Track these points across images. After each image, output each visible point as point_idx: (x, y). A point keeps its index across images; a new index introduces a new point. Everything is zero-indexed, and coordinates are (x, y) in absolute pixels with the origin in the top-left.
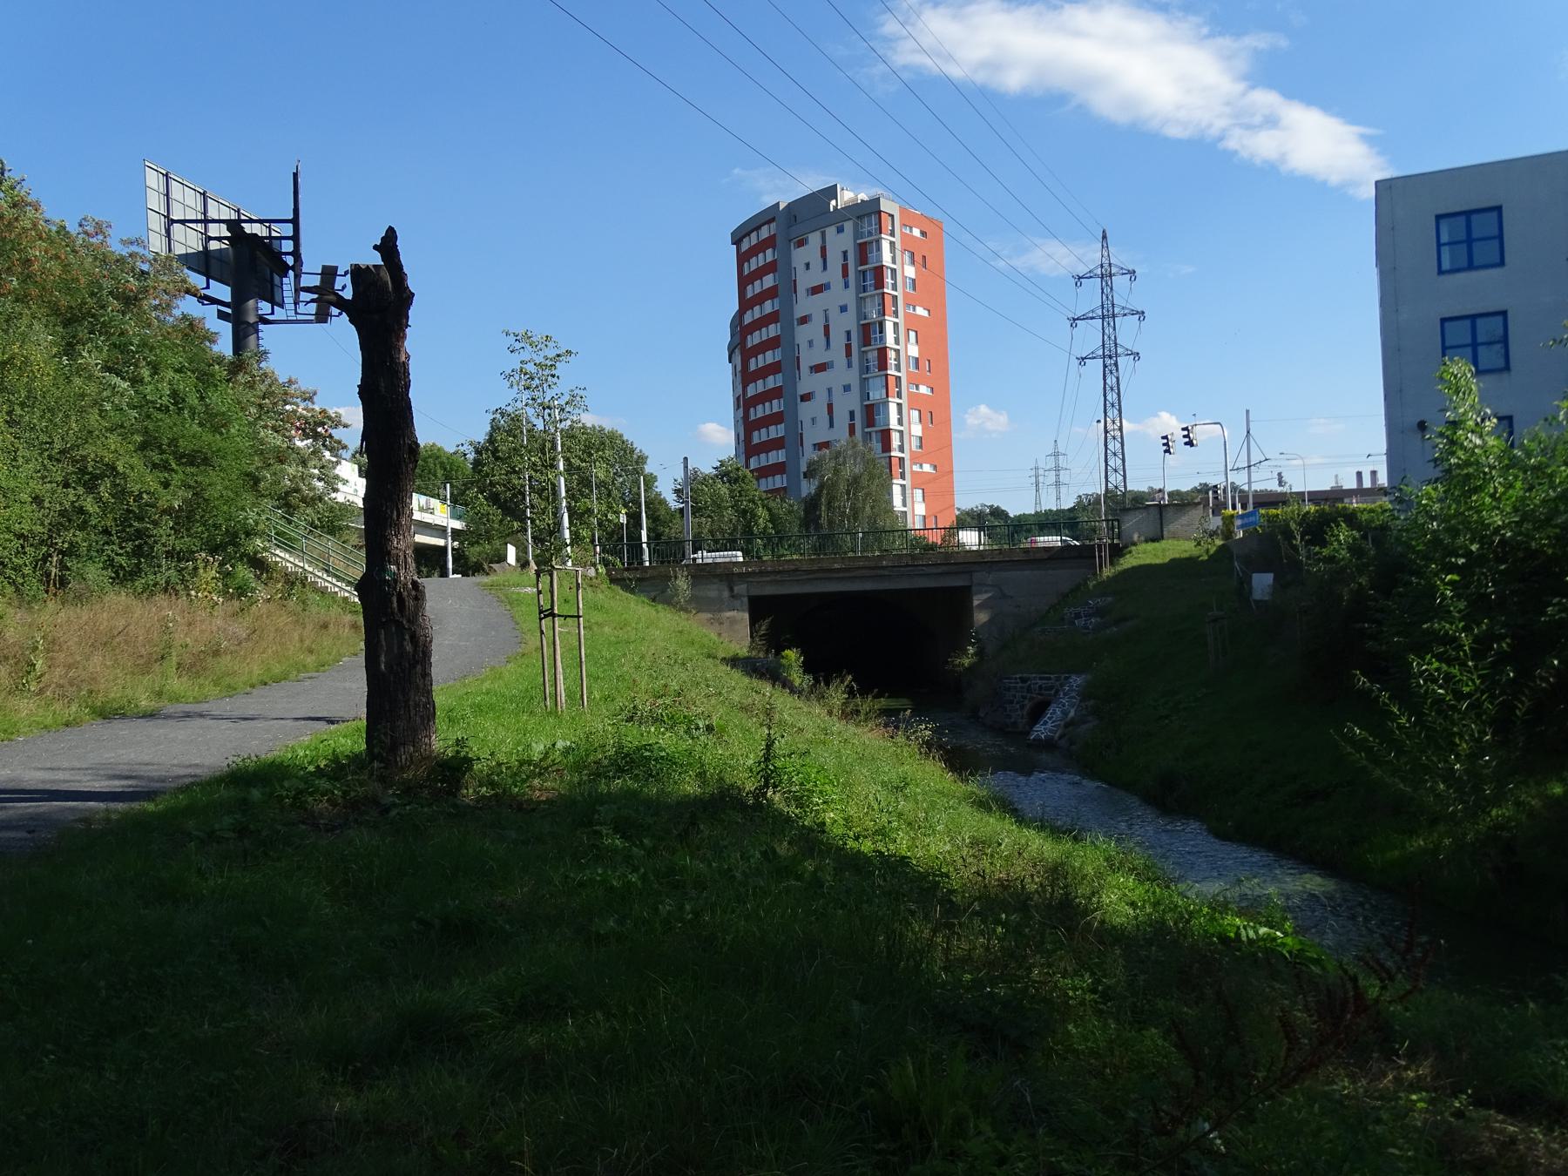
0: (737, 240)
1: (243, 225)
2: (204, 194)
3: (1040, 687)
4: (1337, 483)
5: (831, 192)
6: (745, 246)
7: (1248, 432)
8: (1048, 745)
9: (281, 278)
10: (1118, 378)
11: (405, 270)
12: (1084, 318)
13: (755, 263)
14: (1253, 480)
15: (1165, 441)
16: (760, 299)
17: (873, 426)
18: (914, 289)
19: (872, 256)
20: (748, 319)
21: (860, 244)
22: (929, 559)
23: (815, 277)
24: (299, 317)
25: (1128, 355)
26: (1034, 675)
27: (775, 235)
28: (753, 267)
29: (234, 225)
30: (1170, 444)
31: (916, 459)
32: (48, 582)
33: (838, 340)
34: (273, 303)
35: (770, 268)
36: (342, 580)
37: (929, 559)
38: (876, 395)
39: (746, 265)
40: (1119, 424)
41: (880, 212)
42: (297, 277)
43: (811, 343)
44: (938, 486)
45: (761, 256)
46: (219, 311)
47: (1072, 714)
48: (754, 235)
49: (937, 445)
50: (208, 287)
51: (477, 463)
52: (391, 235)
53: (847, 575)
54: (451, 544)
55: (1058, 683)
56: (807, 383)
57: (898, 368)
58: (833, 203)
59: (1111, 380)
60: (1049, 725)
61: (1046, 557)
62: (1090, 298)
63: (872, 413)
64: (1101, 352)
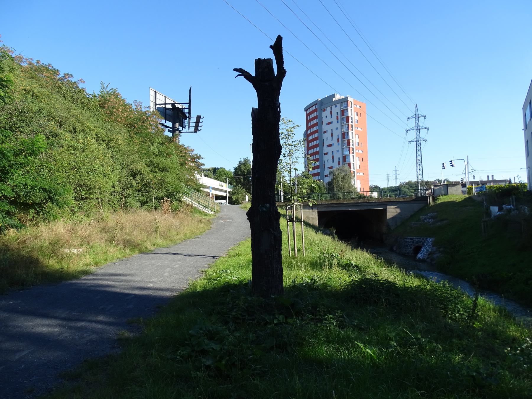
0: (306, 111)
1: (175, 105)
2: (165, 97)
3: (417, 242)
4: (481, 179)
5: (334, 96)
6: (308, 112)
7: (468, 162)
8: (423, 261)
9: (185, 120)
10: (421, 148)
11: (284, 60)
12: (410, 130)
13: (311, 116)
14: (469, 177)
15: (443, 165)
16: (312, 126)
17: (345, 162)
18: (358, 123)
19: (345, 113)
20: (309, 132)
21: (342, 110)
22: (373, 200)
23: (329, 120)
24: (190, 131)
25: (423, 140)
26: (415, 238)
27: (318, 144)
28: (311, 118)
29: (173, 105)
30: (445, 166)
31: (358, 171)
32: (121, 206)
33: (335, 138)
34: (183, 127)
35: (316, 118)
36: (203, 206)
37: (373, 200)
38: (346, 153)
39: (309, 117)
40: (421, 161)
41: (348, 101)
42: (189, 119)
43: (327, 138)
44: (364, 179)
45: (313, 114)
46: (168, 129)
47: (430, 250)
48: (311, 108)
49: (364, 168)
50: (166, 123)
51: (235, 173)
52: (279, 39)
53: (348, 205)
54: (228, 195)
55: (423, 240)
56: (325, 128)
57: (353, 145)
58: (334, 99)
59: (419, 148)
60: (423, 254)
61: (410, 200)
62: (412, 123)
63: (345, 158)
64: (415, 140)
